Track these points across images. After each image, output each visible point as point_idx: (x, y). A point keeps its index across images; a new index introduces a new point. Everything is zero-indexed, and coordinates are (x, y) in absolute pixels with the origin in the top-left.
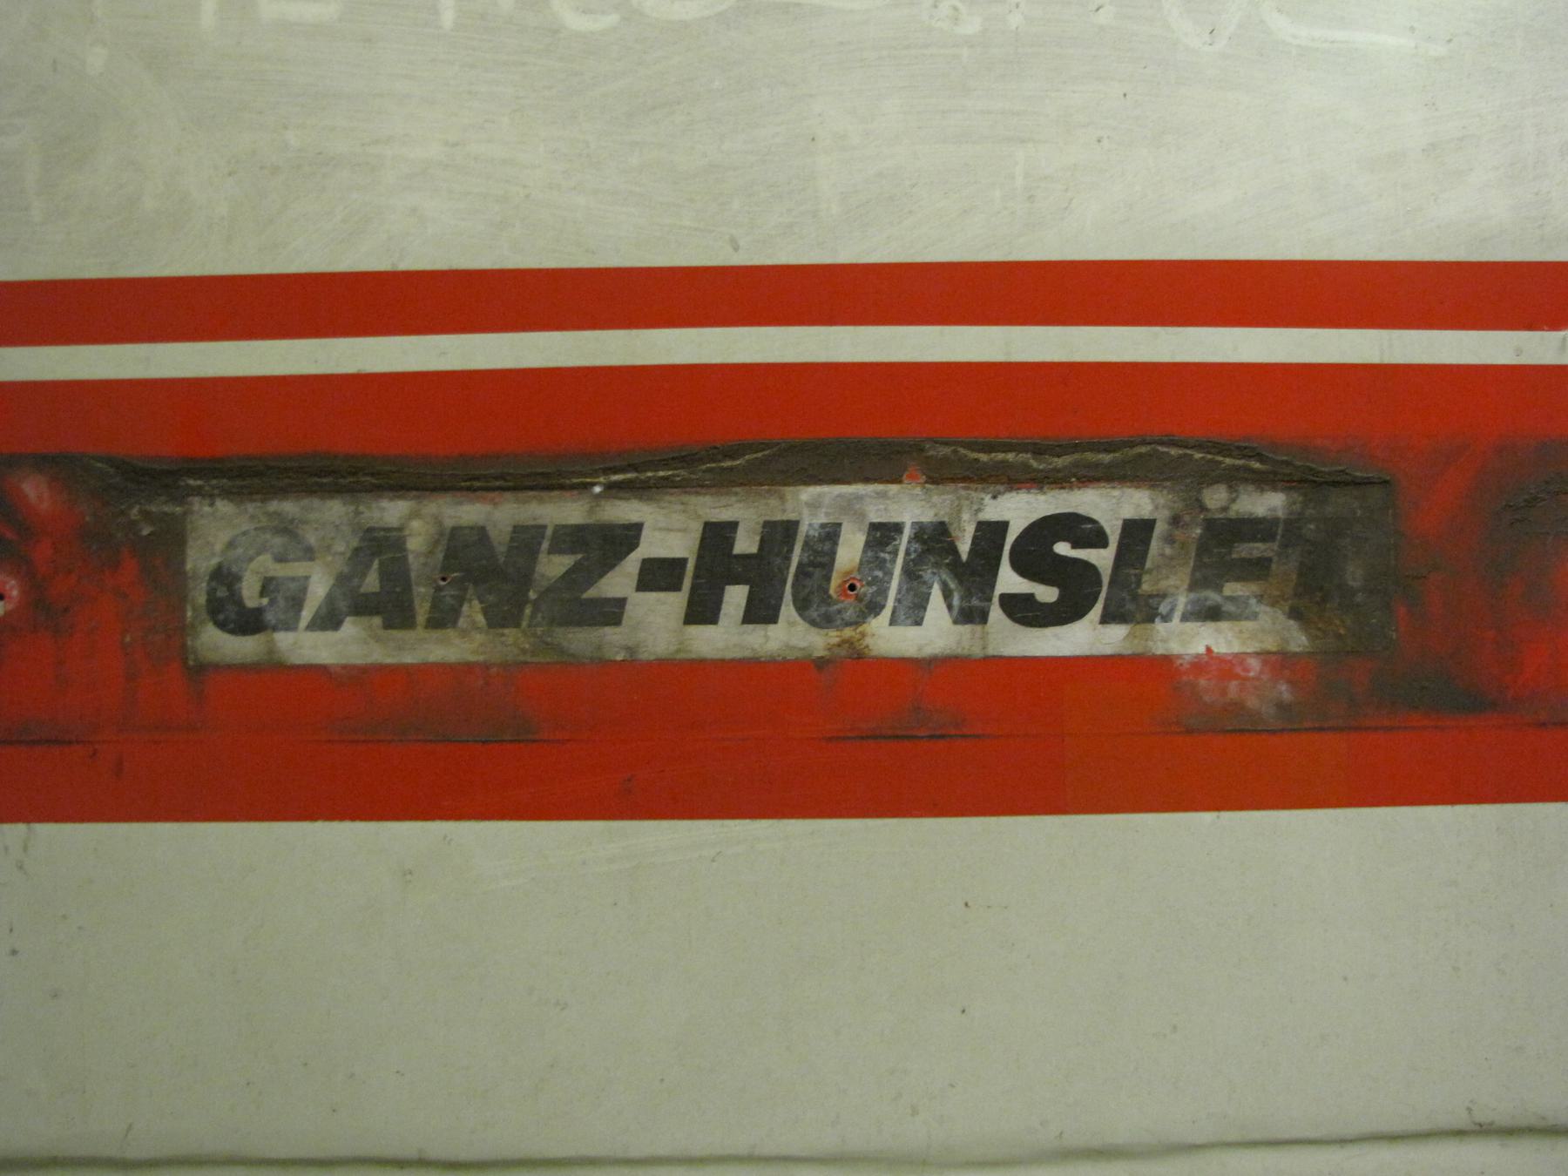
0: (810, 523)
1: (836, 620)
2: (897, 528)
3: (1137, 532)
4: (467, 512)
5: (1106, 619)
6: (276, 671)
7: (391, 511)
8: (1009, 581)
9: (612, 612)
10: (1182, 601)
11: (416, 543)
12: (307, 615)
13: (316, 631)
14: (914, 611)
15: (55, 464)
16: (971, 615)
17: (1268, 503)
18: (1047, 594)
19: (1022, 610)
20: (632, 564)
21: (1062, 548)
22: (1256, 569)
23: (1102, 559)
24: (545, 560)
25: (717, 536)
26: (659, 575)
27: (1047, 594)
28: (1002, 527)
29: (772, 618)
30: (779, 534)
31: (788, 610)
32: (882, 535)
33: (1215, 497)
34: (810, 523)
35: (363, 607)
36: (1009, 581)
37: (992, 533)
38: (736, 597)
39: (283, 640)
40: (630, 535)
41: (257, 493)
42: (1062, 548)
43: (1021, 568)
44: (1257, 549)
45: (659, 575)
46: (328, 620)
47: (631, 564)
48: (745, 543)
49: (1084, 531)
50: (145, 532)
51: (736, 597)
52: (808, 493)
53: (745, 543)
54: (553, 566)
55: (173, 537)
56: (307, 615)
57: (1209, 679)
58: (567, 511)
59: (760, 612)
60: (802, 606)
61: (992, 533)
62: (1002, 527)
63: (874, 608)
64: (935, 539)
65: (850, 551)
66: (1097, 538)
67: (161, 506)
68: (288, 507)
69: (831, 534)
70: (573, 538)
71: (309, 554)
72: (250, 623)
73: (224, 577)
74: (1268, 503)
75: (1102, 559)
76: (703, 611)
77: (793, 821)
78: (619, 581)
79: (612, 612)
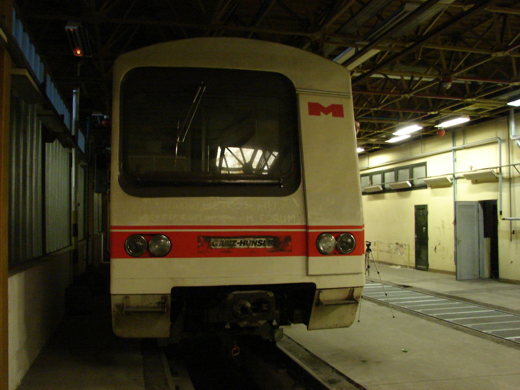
3: (265, 241)
4: (227, 240)
5: (263, 246)
6: (216, 249)
7: (223, 239)
8: (257, 244)
9: (236, 245)
11: (224, 242)
14: (252, 245)
15: (202, 236)
16: (255, 245)
17: (272, 239)
19: (258, 245)
22: (271, 243)
23: (263, 242)
25: (241, 241)
26: (238, 243)
27: (259, 244)
30: (245, 241)
31: (245, 245)
32: (250, 241)
33: (269, 239)
35: (221, 245)
36: (257, 244)
37: (256, 241)
38: (242, 245)
40: (236, 241)
43: (262, 243)
45: (238, 243)
46: (219, 246)
47: (237, 243)
49: (262, 241)
50: (229, 327)
51: (242, 245)
54: (232, 243)
55: (210, 241)
57: (398, 252)
58: (233, 240)
59: (244, 245)
61: (256, 241)
64: (253, 241)
65: (249, 242)
69: (247, 241)
71: (218, 242)
72: (214, 246)
73: (213, 243)
74: (272, 239)
76: (240, 245)
78: (236, 244)
79: (236, 245)
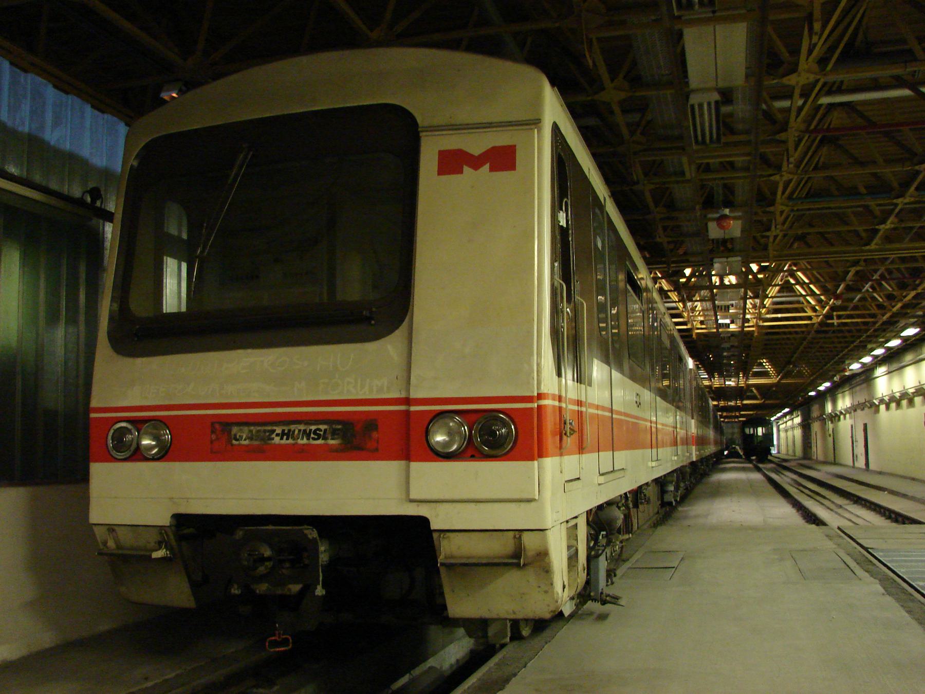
0: (292, 429)
1: (313, 537)
2: (301, 430)
3: (325, 430)
4: (259, 428)
7: (252, 428)
8: (312, 435)
10: (330, 438)
12: (243, 439)
13: (772, 485)
14: (302, 439)
16: (308, 439)
17: (340, 427)
18: (316, 437)
19: (314, 439)
20: (275, 433)
21: (318, 432)
22: (338, 434)
23: (322, 433)
24: (584, 562)
25: (283, 431)
26: (277, 435)
27: (316, 437)
28: (312, 430)
29: (288, 439)
31: (290, 438)
32: (300, 431)
33: (334, 426)
34: (292, 429)
36: (312, 435)
37: (311, 430)
38: (285, 437)
39: (241, 442)
40: (275, 431)
41: (65, 368)
42: (318, 432)
44: (339, 432)
45: (277, 435)
46: (245, 440)
48: (286, 432)
49: (320, 430)
51: (285, 437)
52: (293, 426)
53: (286, 432)
56: (243, 439)
58: (269, 428)
59: (287, 439)
60: (292, 438)
62: (312, 430)
63: (298, 438)
64: (305, 431)
65: (296, 432)
66: (321, 430)
67: (229, 427)
68: (241, 427)
69: (294, 431)
70: (269, 431)
73: (235, 435)
74: (340, 427)
75: (322, 433)
76: (282, 439)
77: (294, 462)
78: (274, 436)
